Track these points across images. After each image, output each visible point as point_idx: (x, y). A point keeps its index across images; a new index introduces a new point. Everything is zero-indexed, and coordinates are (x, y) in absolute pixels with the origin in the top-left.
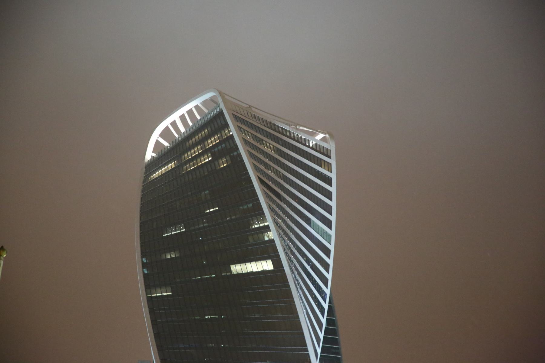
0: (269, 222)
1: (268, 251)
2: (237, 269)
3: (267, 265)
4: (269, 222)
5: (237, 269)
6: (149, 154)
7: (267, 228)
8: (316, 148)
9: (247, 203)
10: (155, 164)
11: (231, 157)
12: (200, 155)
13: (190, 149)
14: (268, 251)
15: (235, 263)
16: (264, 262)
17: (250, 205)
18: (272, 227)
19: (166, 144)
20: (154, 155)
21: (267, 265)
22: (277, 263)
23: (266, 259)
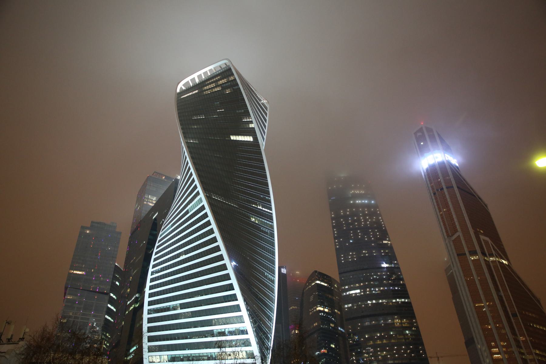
0: (253, 119)
1: (252, 132)
2: (233, 138)
3: (250, 139)
4: (253, 119)
5: (233, 138)
6: (178, 91)
7: (251, 122)
8: (263, 104)
9: (241, 109)
10: (183, 92)
11: (233, 89)
12: (214, 88)
13: (206, 86)
14: (252, 132)
15: (233, 135)
16: (248, 137)
17: (243, 111)
18: (254, 121)
19: (191, 85)
20: (184, 88)
21: (250, 139)
22: (255, 138)
23: (249, 135)
